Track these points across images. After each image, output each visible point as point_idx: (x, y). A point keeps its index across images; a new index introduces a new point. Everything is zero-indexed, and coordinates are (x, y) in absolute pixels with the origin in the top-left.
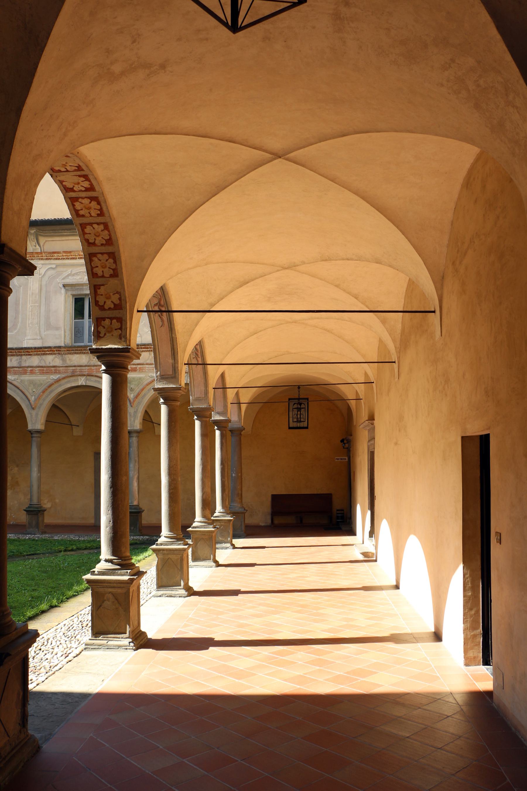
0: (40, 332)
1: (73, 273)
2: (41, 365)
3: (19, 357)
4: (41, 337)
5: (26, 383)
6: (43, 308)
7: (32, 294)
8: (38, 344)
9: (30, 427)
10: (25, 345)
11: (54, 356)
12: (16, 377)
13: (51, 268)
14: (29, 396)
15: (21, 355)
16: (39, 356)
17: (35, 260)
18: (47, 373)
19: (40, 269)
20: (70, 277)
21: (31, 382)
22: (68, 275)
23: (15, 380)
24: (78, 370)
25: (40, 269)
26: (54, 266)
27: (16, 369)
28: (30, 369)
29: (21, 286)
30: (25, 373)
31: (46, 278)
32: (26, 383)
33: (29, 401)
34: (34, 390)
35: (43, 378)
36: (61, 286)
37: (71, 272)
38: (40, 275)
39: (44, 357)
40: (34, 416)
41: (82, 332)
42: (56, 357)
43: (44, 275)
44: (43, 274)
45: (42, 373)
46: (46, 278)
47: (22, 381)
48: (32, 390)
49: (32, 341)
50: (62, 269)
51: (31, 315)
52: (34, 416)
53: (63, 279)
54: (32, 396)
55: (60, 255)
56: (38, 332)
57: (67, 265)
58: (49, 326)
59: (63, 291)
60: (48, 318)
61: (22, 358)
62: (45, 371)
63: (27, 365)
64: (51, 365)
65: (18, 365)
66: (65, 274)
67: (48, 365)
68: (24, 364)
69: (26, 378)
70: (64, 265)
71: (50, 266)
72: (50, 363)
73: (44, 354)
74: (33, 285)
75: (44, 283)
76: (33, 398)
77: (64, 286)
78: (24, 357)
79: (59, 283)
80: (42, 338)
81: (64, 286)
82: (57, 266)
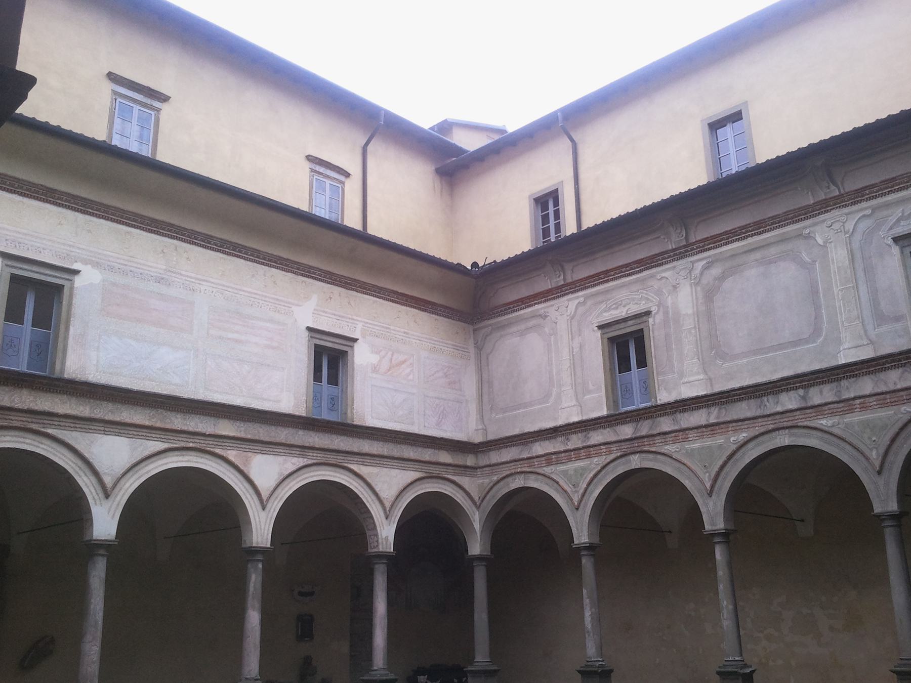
0: (866, 331)
1: (906, 214)
2: (879, 391)
3: (835, 384)
4: (870, 340)
5: (856, 428)
6: (863, 288)
7: (839, 268)
8: (866, 354)
9: (878, 509)
10: (842, 361)
11: (901, 370)
12: (836, 419)
13: (864, 216)
14: (867, 452)
15: (839, 380)
16: (872, 376)
17: (832, 212)
18: (893, 403)
19: (844, 223)
20: (902, 223)
21: (866, 424)
22: (898, 221)
23: (833, 426)
24: (553, 460)
25: (844, 223)
26: (869, 212)
27: (832, 406)
28: (858, 401)
29: (816, 261)
30: (851, 410)
31: (858, 237)
32: (856, 428)
33: (867, 459)
34: (874, 439)
35: (888, 412)
36: (890, 241)
37: (903, 214)
38: (846, 233)
39: (882, 375)
40: (882, 488)
41: (631, 389)
42: (906, 371)
43: (853, 232)
44: (851, 230)
45: (884, 405)
46: (858, 237)
47: (847, 426)
48: (870, 438)
49: (853, 351)
50: (885, 213)
51: (844, 305)
52: (882, 488)
53: (891, 228)
54: (871, 450)
55: (875, 189)
56: (862, 332)
57: (697, 261)
58: (880, 318)
59: (896, 250)
60: (875, 303)
61: (840, 385)
62: (888, 401)
63: (852, 395)
64: (899, 387)
65: (836, 399)
66: (892, 220)
67: (892, 387)
68: (846, 396)
69: (856, 418)
70: (887, 205)
71: (861, 214)
72: (895, 384)
73: (881, 370)
74: (836, 254)
75: (856, 245)
76: (874, 453)
77: (896, 240)
78: (844, 383)
79: (884, 238)
80: (872, 342)
81: (896, 240)
82: (874, 209)
